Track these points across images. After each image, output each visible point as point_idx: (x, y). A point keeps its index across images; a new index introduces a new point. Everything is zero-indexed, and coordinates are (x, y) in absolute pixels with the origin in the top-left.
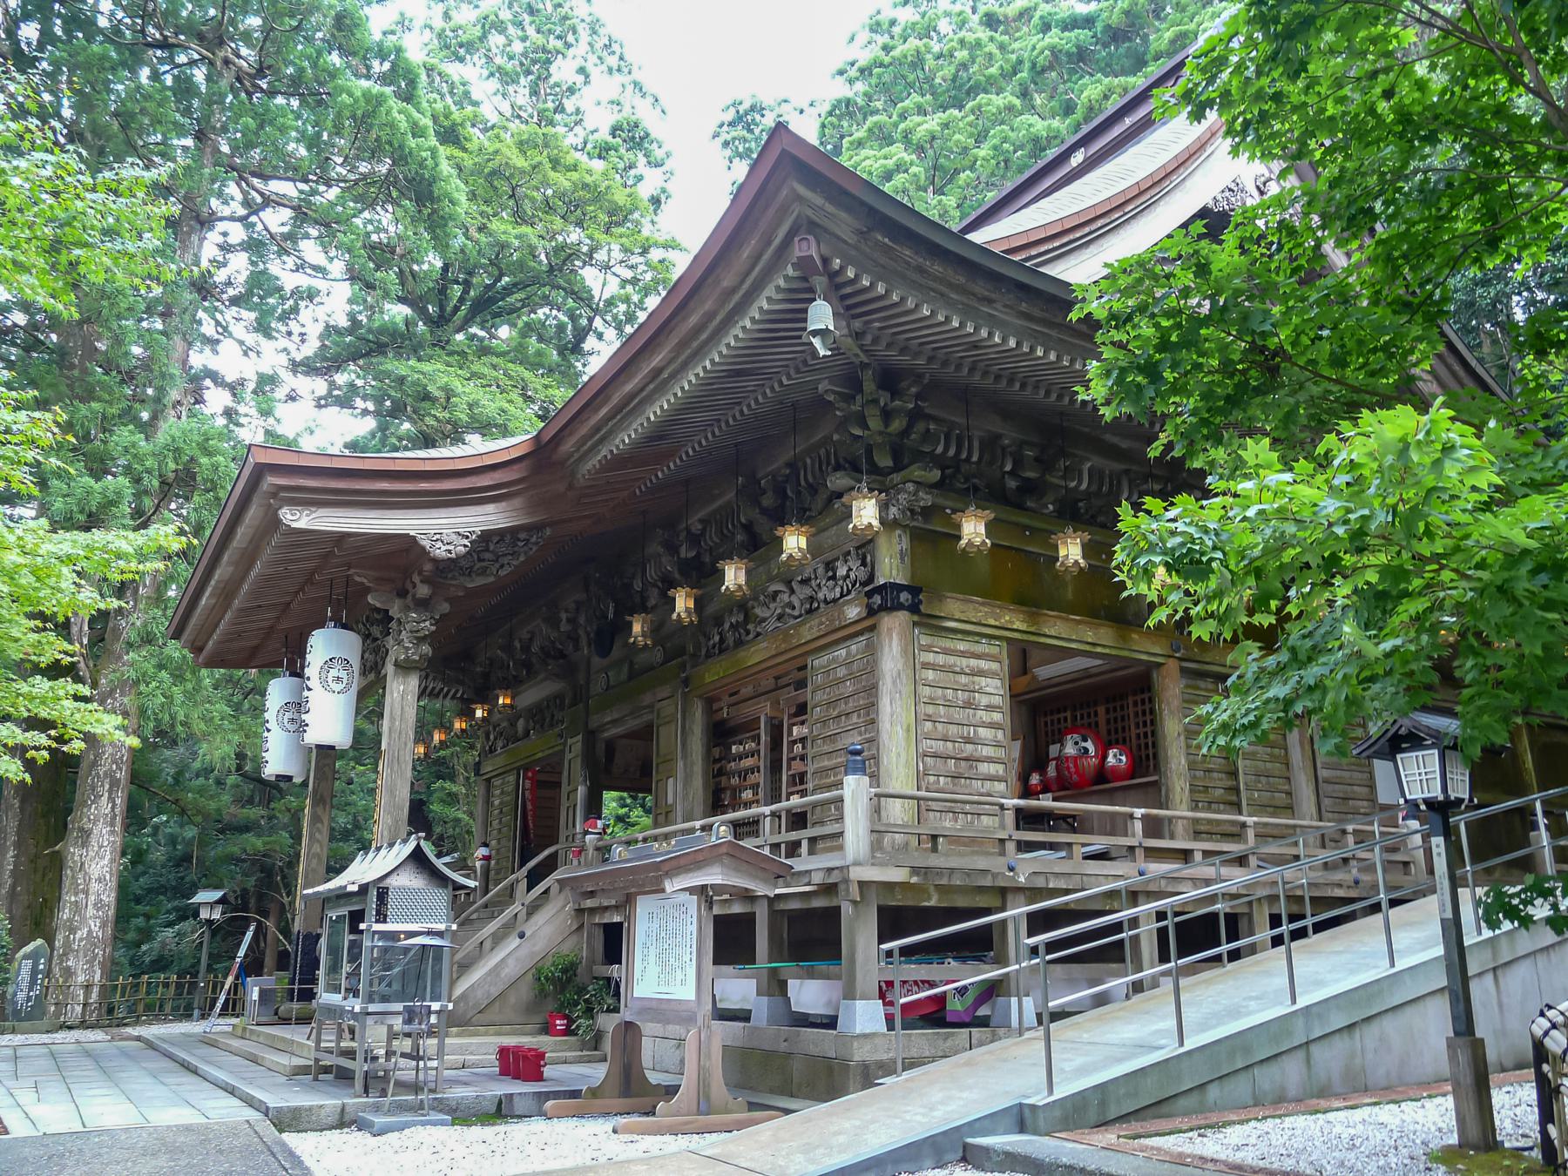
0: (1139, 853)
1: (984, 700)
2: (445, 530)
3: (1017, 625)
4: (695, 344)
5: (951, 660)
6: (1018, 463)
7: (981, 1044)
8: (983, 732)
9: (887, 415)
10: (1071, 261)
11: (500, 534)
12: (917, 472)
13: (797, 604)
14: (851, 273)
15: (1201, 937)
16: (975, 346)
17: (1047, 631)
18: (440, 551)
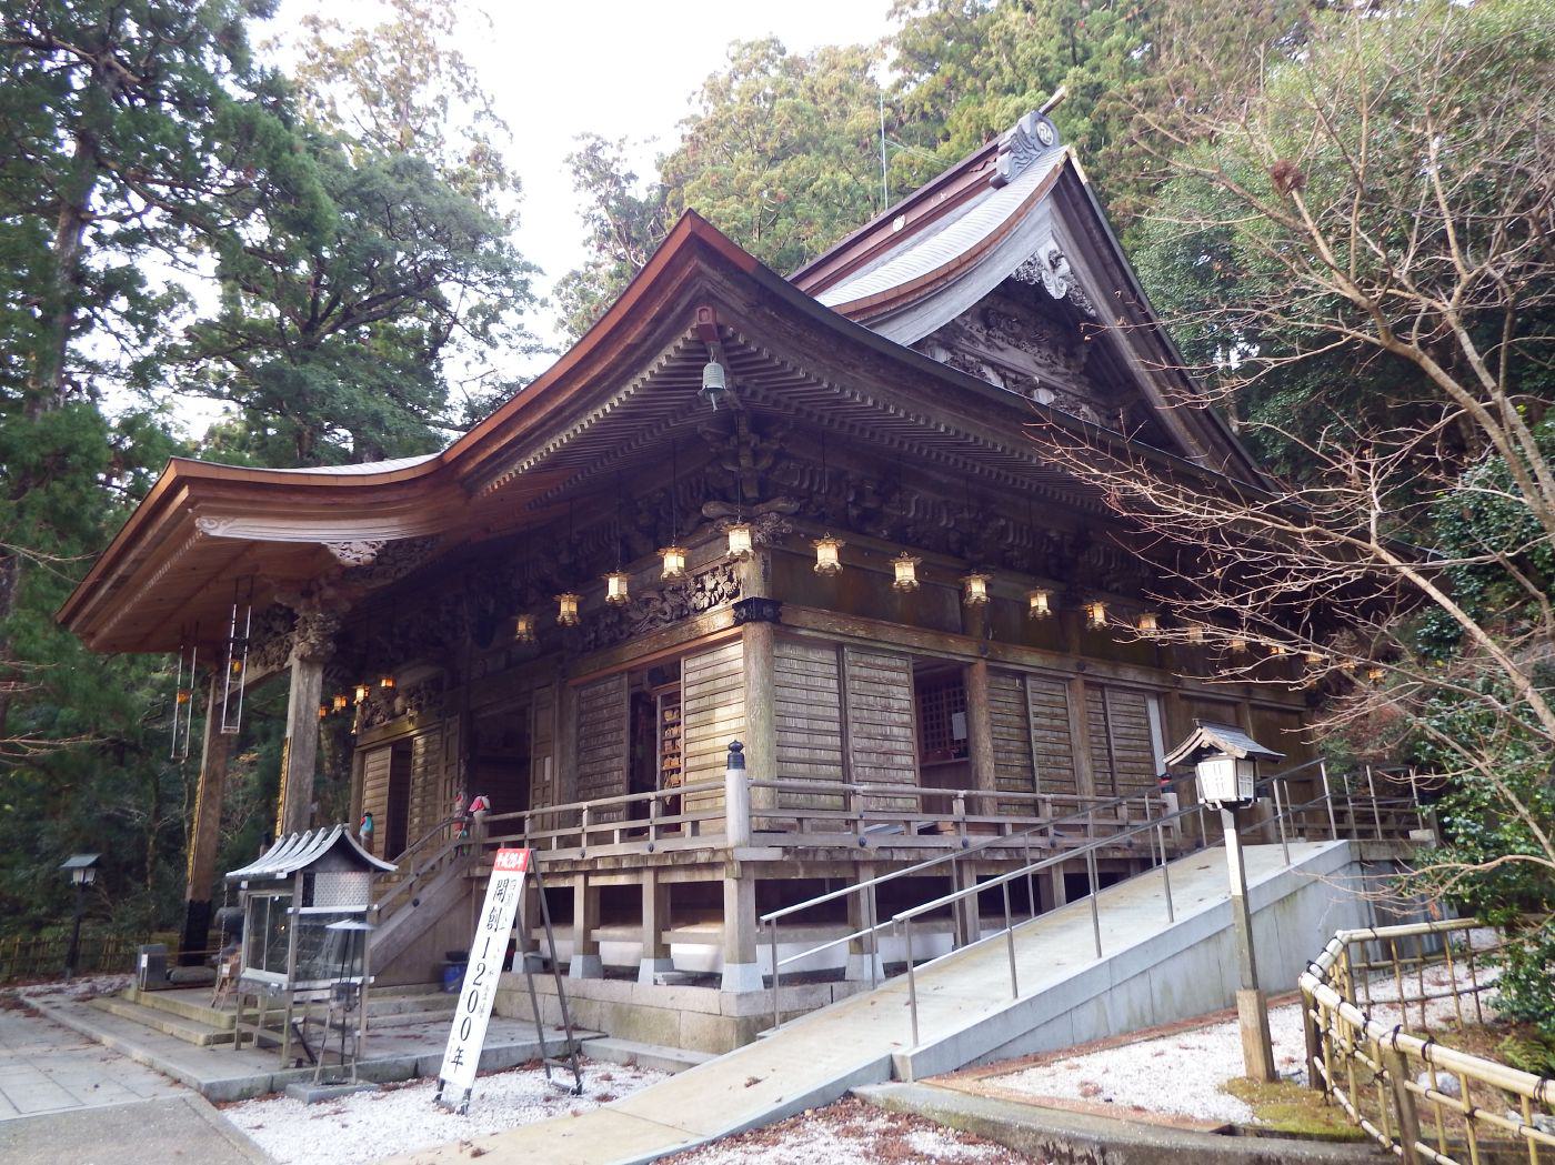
0: (963, 827)
1: (896, 705)
2: (353, 540)
3: (861, 633)
4: (597, 390)
5: (873, 673)
6: (860, 495)
7: (841, 997)
8: (896, 730)
9: (756, 455)
10: (895, 325)
11: (399, 543)
12: (780, 504)
13: (668, 610)
14: (741, 340)
15: (1018, 901)
16: (838, 402)
17: (881, 637)
18: (349, 559)
